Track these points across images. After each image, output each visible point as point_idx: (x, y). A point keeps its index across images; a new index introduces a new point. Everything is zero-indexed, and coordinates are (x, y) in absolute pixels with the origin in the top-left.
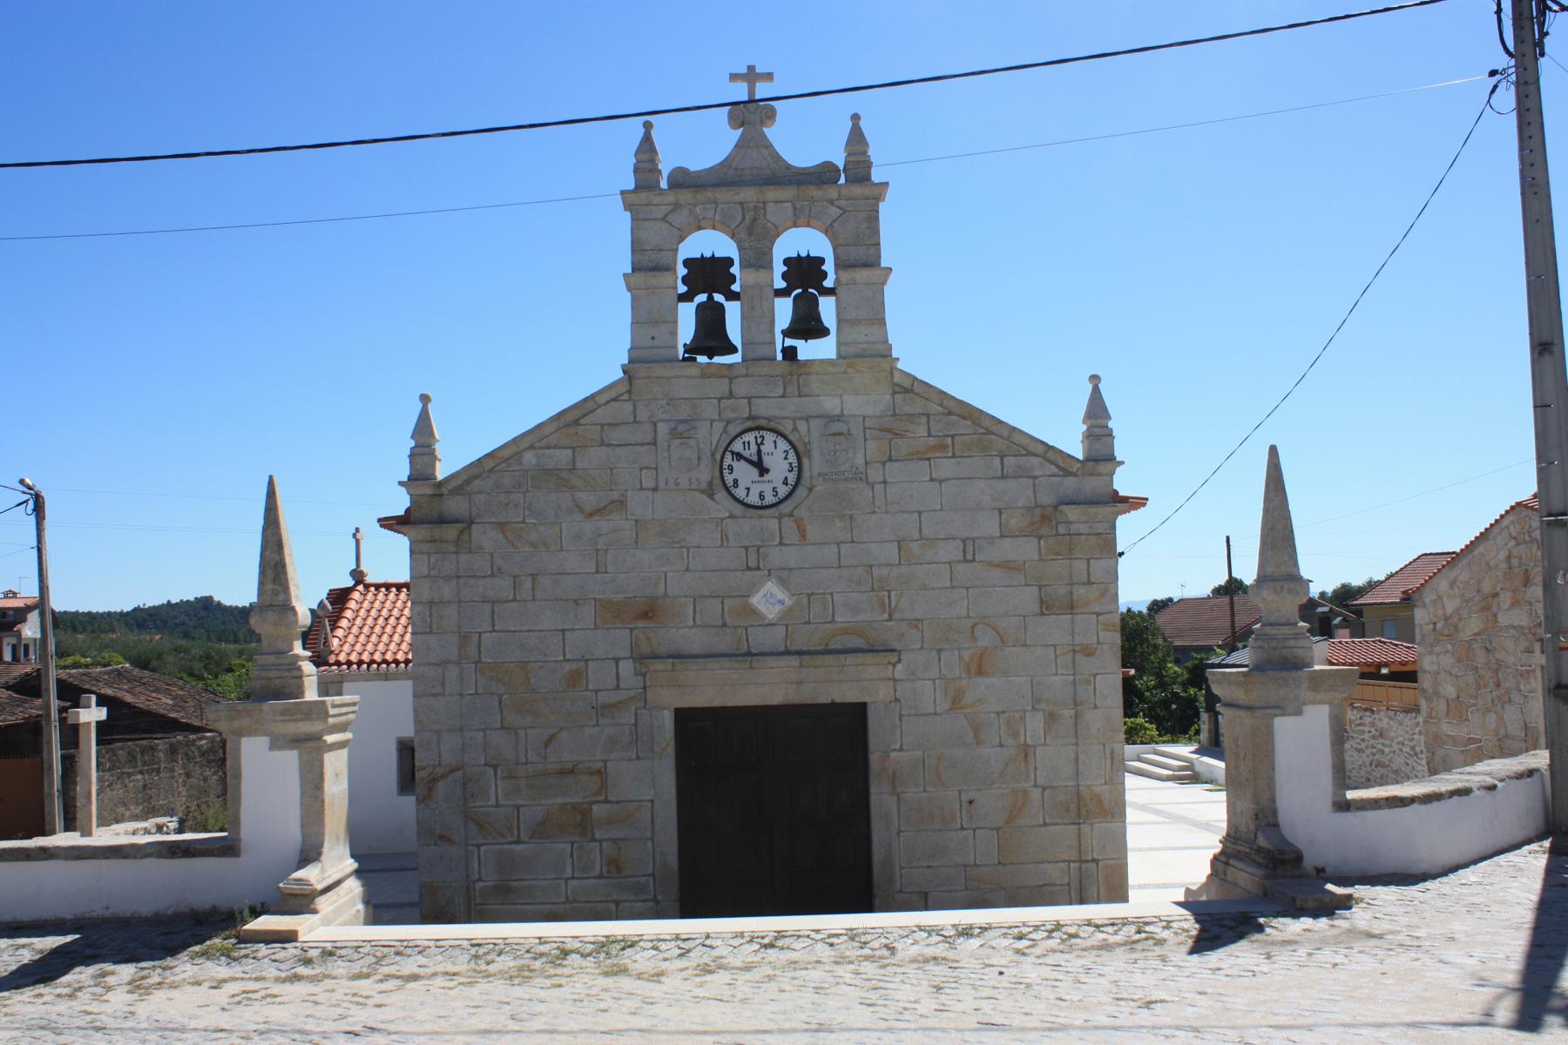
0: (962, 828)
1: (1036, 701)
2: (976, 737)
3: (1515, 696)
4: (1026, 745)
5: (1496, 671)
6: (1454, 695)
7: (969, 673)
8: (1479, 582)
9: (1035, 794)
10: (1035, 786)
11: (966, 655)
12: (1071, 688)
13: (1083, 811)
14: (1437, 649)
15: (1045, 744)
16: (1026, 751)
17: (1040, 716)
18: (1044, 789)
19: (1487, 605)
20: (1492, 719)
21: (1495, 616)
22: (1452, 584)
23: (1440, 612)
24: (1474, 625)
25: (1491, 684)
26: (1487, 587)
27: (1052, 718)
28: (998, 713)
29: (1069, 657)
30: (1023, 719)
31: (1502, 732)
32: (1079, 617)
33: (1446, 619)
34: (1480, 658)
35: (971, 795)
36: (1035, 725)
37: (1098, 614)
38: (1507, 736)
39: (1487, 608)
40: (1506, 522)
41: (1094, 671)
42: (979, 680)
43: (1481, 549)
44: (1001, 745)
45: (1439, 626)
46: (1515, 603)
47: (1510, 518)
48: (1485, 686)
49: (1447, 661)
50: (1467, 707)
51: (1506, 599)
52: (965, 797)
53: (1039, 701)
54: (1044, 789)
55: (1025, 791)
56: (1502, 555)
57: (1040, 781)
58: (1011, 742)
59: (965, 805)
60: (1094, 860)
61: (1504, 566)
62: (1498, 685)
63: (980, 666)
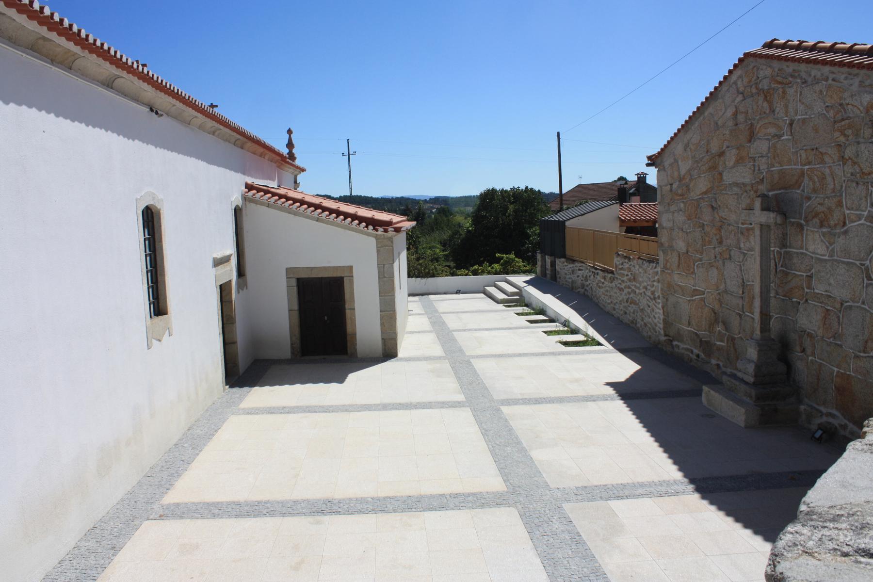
40: (734, 78)
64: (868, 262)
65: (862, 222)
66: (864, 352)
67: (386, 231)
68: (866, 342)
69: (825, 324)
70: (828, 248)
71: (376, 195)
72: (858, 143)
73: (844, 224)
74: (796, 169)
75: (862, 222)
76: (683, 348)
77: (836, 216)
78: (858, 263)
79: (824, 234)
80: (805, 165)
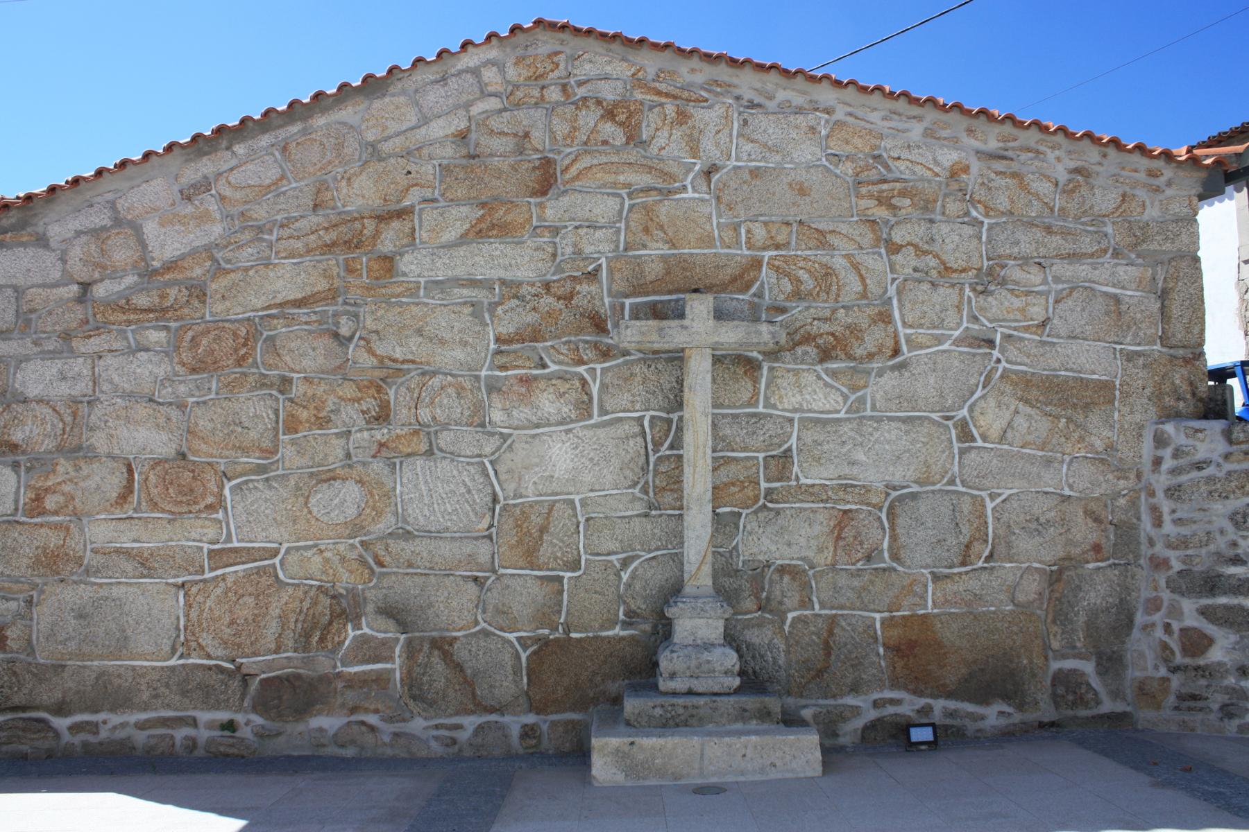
5: (378, 387)
8: (322, 187)
20: (344, 500)
21: (388, 263)
25: (351, 414)
26: (361, 193)
31: (386, 524)
33: (149, 274)
34: (304, 355)
40: (470, 60)
43: (348, 113)
45: (100, 291)
48: (323, 422)
49: (147, 370)
62: (383, 416)
64: (964, 412)
65: (946, 346)
66: (963, 564)
67: (1111, 447)
68: (968, 546)
69: (839, 538)
70: (846, 398)
71: (1226, 128)
72: (932, 221)
73: (896, 352)
74: (731, 257)
75: (946, 346)
76: (210, 725)
77: (874, 338)
78: (934, 416)
79: (834, 374)
80: (765, 249)
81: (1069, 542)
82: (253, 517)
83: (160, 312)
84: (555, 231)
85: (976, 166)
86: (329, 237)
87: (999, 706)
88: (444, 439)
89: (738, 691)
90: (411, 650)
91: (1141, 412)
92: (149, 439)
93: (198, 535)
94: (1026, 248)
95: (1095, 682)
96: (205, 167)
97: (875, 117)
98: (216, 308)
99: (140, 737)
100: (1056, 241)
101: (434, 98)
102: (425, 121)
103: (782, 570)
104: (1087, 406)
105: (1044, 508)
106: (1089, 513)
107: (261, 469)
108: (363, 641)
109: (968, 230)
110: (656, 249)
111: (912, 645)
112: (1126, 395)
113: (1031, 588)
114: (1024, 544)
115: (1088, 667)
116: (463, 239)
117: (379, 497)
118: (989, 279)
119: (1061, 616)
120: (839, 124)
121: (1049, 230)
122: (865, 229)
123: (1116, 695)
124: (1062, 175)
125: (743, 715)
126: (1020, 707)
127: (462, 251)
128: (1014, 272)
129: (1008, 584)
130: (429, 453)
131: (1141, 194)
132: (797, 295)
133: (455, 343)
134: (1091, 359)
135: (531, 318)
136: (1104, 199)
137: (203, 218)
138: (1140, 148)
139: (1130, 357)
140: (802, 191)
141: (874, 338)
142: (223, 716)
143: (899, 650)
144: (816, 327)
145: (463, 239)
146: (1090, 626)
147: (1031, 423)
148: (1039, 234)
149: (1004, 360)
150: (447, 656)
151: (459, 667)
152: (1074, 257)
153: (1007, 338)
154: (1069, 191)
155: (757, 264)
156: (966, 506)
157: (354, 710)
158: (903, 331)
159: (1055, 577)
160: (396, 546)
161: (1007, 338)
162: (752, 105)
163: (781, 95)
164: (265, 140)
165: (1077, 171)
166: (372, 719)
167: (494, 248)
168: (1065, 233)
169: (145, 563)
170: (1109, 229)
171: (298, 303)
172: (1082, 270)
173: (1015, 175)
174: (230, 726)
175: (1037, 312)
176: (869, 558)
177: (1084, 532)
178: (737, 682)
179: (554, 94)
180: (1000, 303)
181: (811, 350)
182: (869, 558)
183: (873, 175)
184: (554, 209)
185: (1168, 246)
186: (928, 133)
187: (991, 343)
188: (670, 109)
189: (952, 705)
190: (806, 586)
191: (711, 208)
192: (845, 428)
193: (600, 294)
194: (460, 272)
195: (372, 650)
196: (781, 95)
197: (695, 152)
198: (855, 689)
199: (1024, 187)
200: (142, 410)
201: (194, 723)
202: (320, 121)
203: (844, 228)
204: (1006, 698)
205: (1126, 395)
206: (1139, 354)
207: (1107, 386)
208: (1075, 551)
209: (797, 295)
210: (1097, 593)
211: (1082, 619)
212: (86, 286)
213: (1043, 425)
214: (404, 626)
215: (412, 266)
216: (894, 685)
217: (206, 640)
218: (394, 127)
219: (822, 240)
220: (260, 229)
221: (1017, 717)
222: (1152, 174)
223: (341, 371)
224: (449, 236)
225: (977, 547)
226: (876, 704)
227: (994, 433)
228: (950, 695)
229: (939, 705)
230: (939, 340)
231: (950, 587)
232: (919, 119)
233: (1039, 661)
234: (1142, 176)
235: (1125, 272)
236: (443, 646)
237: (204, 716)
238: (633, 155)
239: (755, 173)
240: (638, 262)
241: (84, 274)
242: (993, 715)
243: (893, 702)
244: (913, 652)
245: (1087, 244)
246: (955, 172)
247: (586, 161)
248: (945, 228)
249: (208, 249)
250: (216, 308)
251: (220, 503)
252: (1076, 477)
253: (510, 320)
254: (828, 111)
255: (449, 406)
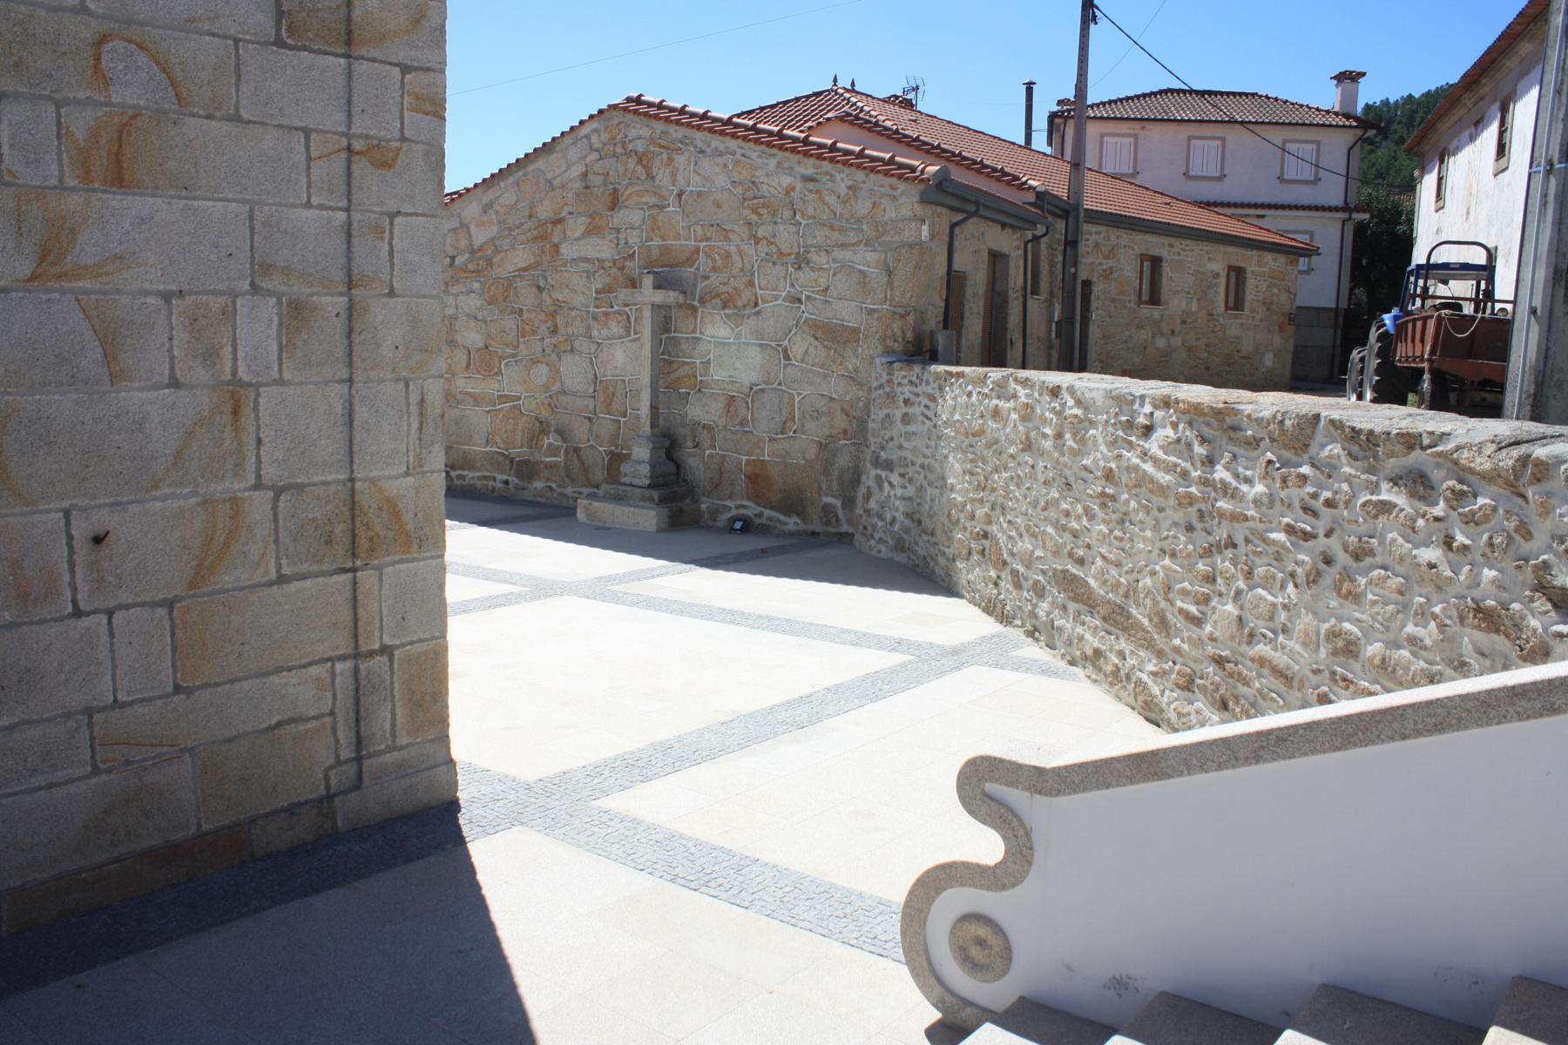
0: (78, 613)
1: (262, 268)
2: (109, 358)
3: (581, 344)
4: (235, 381)
5: (553, 315)
6: (481, 344)
7: (87, 177)
8: (532, 206)
9: (259, 505)
10: (258, 486)
11: (80, 124)
12: (339, 243)
13: (363, 542)
14: (454, 290)
15: (280, 382)
16: (236, 399)
17: (268, 310)
18: (278, 492)
19: (546, 235)
20: (541, 373)
21: (556, 246)
22: (486, 209)
23: (463, 243)
24: (520, 257)
25: (543, 328)
26: (545, 211)
27: (296, 314)
28: (167, 297)
29: (339, 163)
30: (229, 313)
31: (556, 387)
32: (362, 67)
33: (473, 252)
34: (527, 298)
35: (101, 519)
36: (257, 327)
37: (406, 69)
38: (564, 393)
39: (543, 237)
40: (586, 130)
41: (392, 206)
42: (115, 200)
43: (540, 164)
44: (175, 383)
45: (458, 261)
46: (592, 231)
47: (594, 125)
48: (534, 332)
49: (472, 302)
50: (501, 358)
51: (577, 226)
52: (82, 529)
53: (267, 268)
54: (278, 492)
55: (235, 501)
56: (576, 171)
57: (270, 473)
58: (201, 374)
59: (82, 547)
60: (387, 650)
61: (578, 185)
62: (554, 331)
63: (117, 159)
73: (756, 304)
77: (746, 295)
79: (728, 316)
81: (832, 427)
82: (511, 380)
83: (477, 272)
84: (618, 231)
85: (799, 185)
86: (535, 233)
87: (795, 519)
88: (577, 344)
89: (649, 487)
90: (567, 452)
91: (870, 348)
92: (474, 338)
93: (491, 388)
94: (820, 240)
95: (840, 513)
96: (491, 194)
97: (754, 155)
98: (497, 272)
99: (478, 483)
100: (836, 234)
101: (573, 153)
102: (569, 167)
103: (704, 426)
104: (845, 343)
105: (822, 405)
106: (843, 410)
107: (514, 356)
108: (550, 445)
109: (793, 229)
110: (657, 242)
111: (757, 476)
112: (866, 337)
113: (813, 451)
114: (811, 425)
115: (838, 503)
116: (582, 237)
117: (555, 372)
118: (801, 261)
119: (826, 471)
120: (737, 162)
121: (832, 228)
122: (745, 229)
123: (849, 522)
124: (843, 190)
125: (643, 498)
126: (804, 521)
127: (582, 242)
128: (813, 257)
129: (803, 447)
130: (572, 350)
131: (885, 202)
132: (714, 269)
133: (577, 291)
134: (847, 313)
135: (608, 280)
136: (862, 207)
137: (490, 223)
138: (582, 122)
139: (870, 312)
140: (718, 205)
141: (746, 295)
142: (505, 477)
143: (752, 479)
144: (722, 289)
145: (582, 237)
146: (840, 478)
147: (818, 352)
148: (827, 231)
149: (808, 312)
150: (579, 456)
151: (582, 463)
152: (844, 246)
153: (808, 297)
154: (844, 203)
155: (697, 250)
156: (786, 401)
157: (548, 480)
158: (759, 292)
159: (822, 446)
160: (562, 398)
161: (808, 297)
162: (702, 152)
163: (714, 144)
164: (511, 180)
165: (849, 188)
166: (554, 485)
167: (594, 240)
168: (840, 230)
169: (476, 400)
170: (864, 227)
171: (525, 269)
172: (847, 255)
173: (818, 192)
174: (506, 482)
175: (823, 282)
176: (741, 424)
177: (840, 422)
178: (647, 482)
179: (619, 150)
180: (806, 276)
181: (718, 301)
182: (741, 424)
183: (750, 194)
184: (618, 218)
185: (897, 238)
186: (779, 164)
187: (799, 300)
188: (665, 156)
189: (773, 514)
190: (713, 437)
191: (679, 218)
192: (734, 348)
193: (634, 267)
194: (583, 254)
195: (553, 451)
196: (714, 144)
197: (674, 182)
198: (731, 497)
199: (822, 200)
200: (472, 323)
201: (494, 479)
202: (531, 168)
203: (736, 228)
204: (798, 514)
205: (866, 337)
206: (875, 310)
207: (856, 331)
208: (835, 432)
209: (714, 269)
210: (843, 461)
211: (836, 474)
212: (453, 258)
213: (823, 352)
214: (564, 439)
215: (565, 250)
216: (749, 499)
217: (498, 439)
218: (558, 171)
219: (726, 235)
220: (511, 229)
221: (802, 527)
222: (893, 188)
223: (540, 306)
224: (578, 234)
225: (789, 424)
226: (738, 507)
227: (799, 357)
228: (772, 508)
229: (767, 512)
230: (776, 298)
231: (776, 446)
232: (774, 155)
233: (815, 495)
234: (886, 190)
235: (872, 257)
236: (577, 450)
237: (500, 477)
238: (648, 185)
239: (700, 194)
240: (649, 248)
241: (451, 252)
242: (792, 523)
243: (746, 507)
244: (757, 480)
245: (852, 237)
246: (789, 190)
247: (631, 189)
248: (781, 228)
249: (493, 239)
250: (497, 272)
251: (499, 373)
252: (836, 387)
253: (601, 281)
254: (734, 154)
255: (577, 328)
